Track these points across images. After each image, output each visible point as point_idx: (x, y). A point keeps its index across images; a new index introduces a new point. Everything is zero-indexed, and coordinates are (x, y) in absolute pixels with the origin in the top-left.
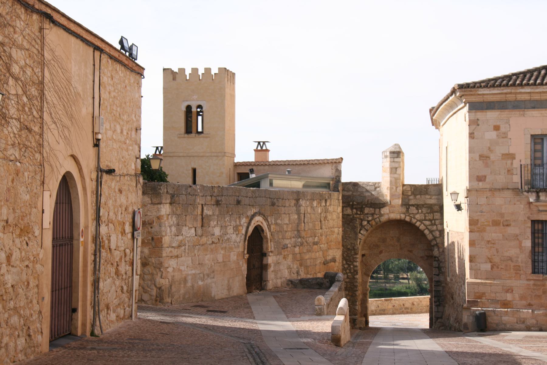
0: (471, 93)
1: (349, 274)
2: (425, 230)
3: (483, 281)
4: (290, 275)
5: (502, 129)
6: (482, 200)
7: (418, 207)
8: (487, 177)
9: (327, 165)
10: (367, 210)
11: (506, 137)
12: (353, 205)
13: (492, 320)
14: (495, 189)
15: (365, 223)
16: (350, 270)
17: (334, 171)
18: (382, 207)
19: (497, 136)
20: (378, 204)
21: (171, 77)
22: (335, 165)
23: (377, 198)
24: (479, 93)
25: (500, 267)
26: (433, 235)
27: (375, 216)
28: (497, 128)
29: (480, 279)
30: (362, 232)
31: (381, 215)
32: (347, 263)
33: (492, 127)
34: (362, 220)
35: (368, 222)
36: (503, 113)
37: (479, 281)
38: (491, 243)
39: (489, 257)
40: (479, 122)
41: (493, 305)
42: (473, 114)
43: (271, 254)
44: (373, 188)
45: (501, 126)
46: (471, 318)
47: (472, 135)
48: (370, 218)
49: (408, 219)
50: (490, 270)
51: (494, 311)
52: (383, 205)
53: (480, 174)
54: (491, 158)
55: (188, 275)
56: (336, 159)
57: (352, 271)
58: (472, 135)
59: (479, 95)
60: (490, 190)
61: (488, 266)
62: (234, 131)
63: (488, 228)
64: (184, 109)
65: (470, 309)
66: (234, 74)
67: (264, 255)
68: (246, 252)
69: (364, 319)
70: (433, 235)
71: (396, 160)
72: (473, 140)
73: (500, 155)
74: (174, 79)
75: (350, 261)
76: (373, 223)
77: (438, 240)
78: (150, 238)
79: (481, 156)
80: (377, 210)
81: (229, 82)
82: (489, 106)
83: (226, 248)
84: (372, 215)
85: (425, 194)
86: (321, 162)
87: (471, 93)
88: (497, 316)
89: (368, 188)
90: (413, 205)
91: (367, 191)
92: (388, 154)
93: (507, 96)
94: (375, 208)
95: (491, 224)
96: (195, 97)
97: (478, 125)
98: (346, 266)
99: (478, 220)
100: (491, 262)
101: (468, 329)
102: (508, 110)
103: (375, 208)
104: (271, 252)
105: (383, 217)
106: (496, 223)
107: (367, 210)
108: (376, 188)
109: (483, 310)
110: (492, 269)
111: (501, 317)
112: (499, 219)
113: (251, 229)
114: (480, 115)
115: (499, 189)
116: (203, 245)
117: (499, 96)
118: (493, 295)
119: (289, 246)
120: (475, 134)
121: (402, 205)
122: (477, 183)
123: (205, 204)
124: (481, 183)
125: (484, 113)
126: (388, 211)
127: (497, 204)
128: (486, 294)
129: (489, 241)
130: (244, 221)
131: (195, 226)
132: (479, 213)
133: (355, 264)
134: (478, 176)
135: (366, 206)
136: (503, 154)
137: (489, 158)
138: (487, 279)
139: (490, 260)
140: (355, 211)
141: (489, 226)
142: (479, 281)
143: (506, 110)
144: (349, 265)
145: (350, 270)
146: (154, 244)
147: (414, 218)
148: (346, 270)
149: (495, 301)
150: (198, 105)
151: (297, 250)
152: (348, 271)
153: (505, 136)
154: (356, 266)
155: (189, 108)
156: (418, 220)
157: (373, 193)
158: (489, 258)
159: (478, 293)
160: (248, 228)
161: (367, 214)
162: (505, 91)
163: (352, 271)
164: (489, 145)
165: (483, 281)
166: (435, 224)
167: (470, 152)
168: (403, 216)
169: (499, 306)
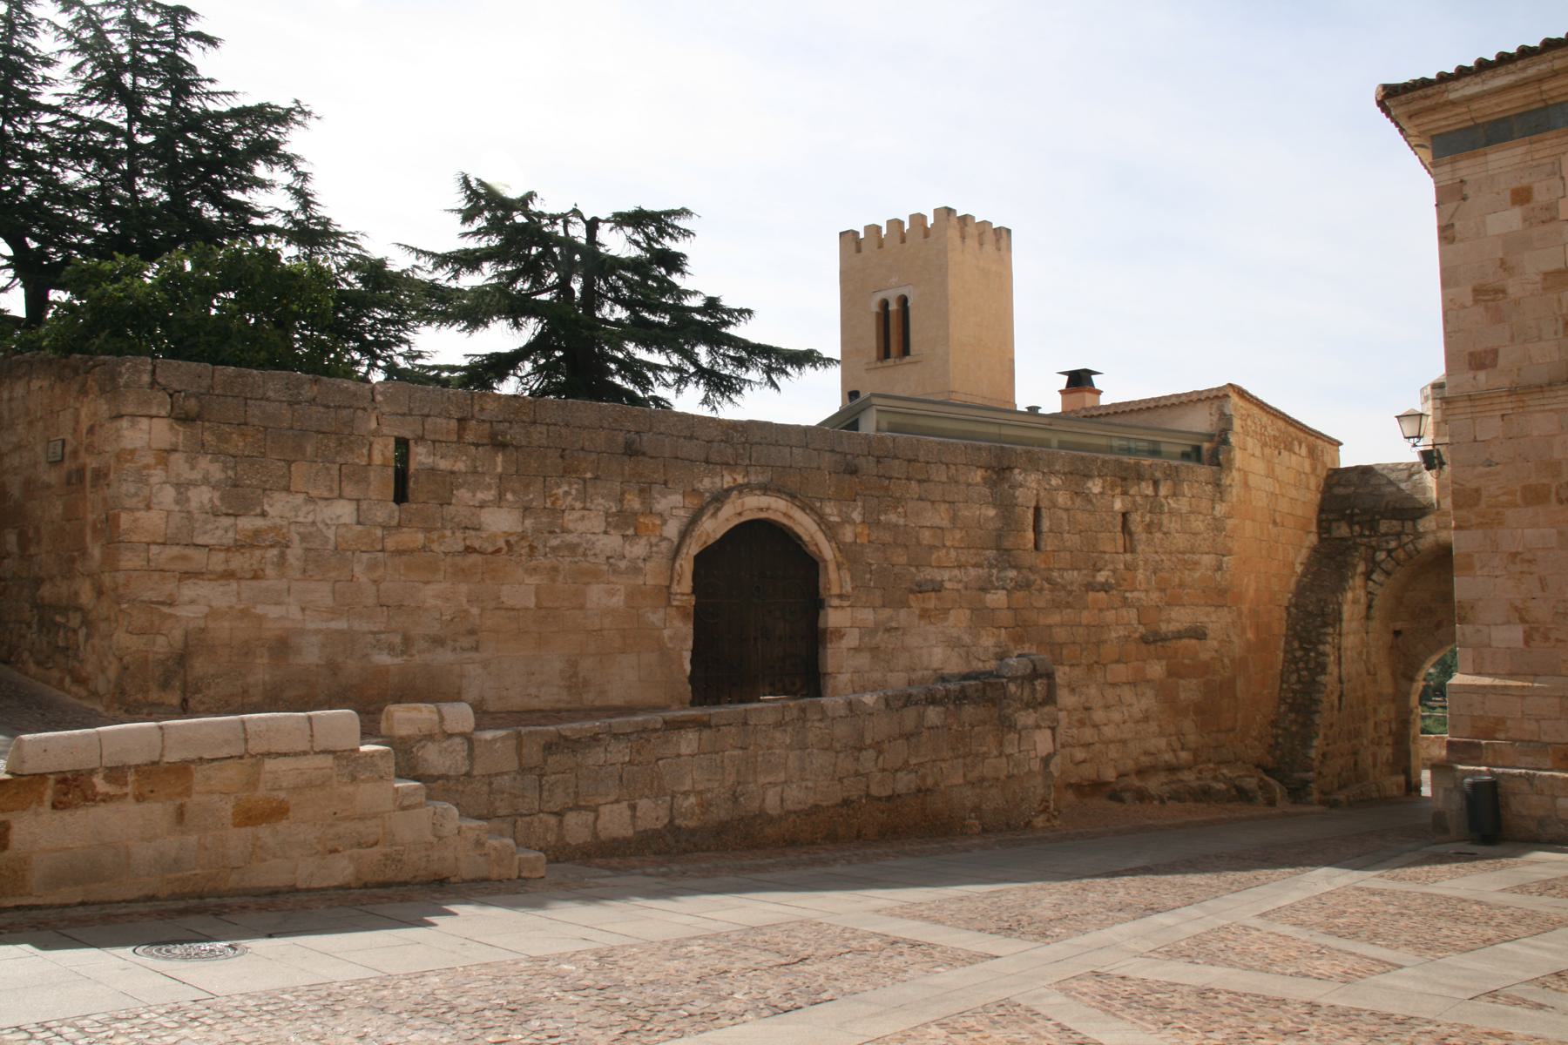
0: (1427, 103)
1: (1304, 673)
3: (1497, 682)
4: (968, 662)
5: (1541, 197)
6: (1490, 427)
8: (1501, 352)
9: (1199, 405)
10: (1384, 526)
11: (1553, 219)
12: (1352, 515)
13: (1525, 806)
14: (1529, 387)
15: (1381, 556)
16: (1306, 663)
17: (1215, 418)
18: (1420, 517)
19: (1525, 220)
20: (1411, 511)
21: (853, 246)
22: (1216, 403)
23: (1410, 498)
24: (1452, 96)
25: (1554, 635)
27: (1405, 539)
28: (1521, 196)
29: (1489, 675)
30: (1374, 577)
31: (1418, 535)
32: (1301, 648)
33: (1508, 193)
34: (1375, 549)
35: (1389, 552)
36: (1538, 146)
37: (1486, 681)
38: (1524, 561)
39: (1518, 603)
40: (1467, 190)
41: (1529, 759)
42: (1447, 168)
43: (835, 602)
44: (1406, 474)
45: (1536, 187)
47: (1448, 233)
48: (1393, 544)
50: (1521, 644)
51: (1529, 779)
52: (1422, 511)
53: (1479, 348)
54: (1510, 290)
56: (1219, 389)
57: (1312, 665)
58: (1447, 233)
59: (1453, 103)
60: (1512, 392)
61: (1516, 634)
62: (1012, 351)
63: (1509, 512)
64: (874, 307)
66: (1009, 231)
67: (815, 604)
69: (1401, 779)
72: (1450, 247)
73: (1538, 278)
74: (859, 250)
75: (1310, 642)
76: (1401, 555)
79: (1478, 292)
80: (1409, 524)
81: (972, 243)
82: (1495, 133)
83: (555, 569)
84: (1398, 535)
86: (1183, 399)
87: (1427, 103)
88: (1541, 793)
89: (1393, 476)
91: (1390, 483)
92: (1429, 391)
93: (1545, 87)
94: (1403, 521)
95: (1519, 501)
96: (894, 280)
97: (1464, 199)
98: (1299, 654)
99: (1477, 490)
100: (1523, 620)
102: (1555, 132)
103: (1403, 521)
104: (840, 596)
105: (1422, 541)
106: (1535, 496)
107: (1384, 526)
108: (1411, 475)
109: (1492, 773)
110: (1526, 642)
111: (1554, 797)
112: (1544, 481)
113: (714, 527)
114: (1467, 168)
115: (1540, 388)
117: (1517, 94)
118: (1533, 726)
119: (948, 585)
120: (1457, 226)
122: (1471, 374)
123: (421, 439)
124: (1482, 375)
125: (1481, 160)
126: (1433, 525)
127: (1535, 433)
128: (1509, 723)
129: (1514, 555)
130: (672, 503)
132: (1481, 469)
133: (1321, 647)
134: (1471, 354)
135: (1383, 517)
136: (1546, 275)
137: (1503, 291)
138: (1512, 675)
139: (1520, 614)
140: (1357, 528)
141: (1514, 505)
142: (1486, 681)
143: (1549, 135)
144: (1307, 651)
145: (1306, 663)
148: (1296, 664)
149: (1535, 747)
152: (1301, 665)
153: (1550, 215)
154: (1324, 654)
157: (1403, 486)
158: (1516, 609)
159: (1481, 718)
160: (694, 521)
161: (1386, 534)
162: (1531, 72)
163: (1312, 665)
164: (1500, 255)
165: (1497, 682)
167: (1445, 284)
169: (1549, 764)
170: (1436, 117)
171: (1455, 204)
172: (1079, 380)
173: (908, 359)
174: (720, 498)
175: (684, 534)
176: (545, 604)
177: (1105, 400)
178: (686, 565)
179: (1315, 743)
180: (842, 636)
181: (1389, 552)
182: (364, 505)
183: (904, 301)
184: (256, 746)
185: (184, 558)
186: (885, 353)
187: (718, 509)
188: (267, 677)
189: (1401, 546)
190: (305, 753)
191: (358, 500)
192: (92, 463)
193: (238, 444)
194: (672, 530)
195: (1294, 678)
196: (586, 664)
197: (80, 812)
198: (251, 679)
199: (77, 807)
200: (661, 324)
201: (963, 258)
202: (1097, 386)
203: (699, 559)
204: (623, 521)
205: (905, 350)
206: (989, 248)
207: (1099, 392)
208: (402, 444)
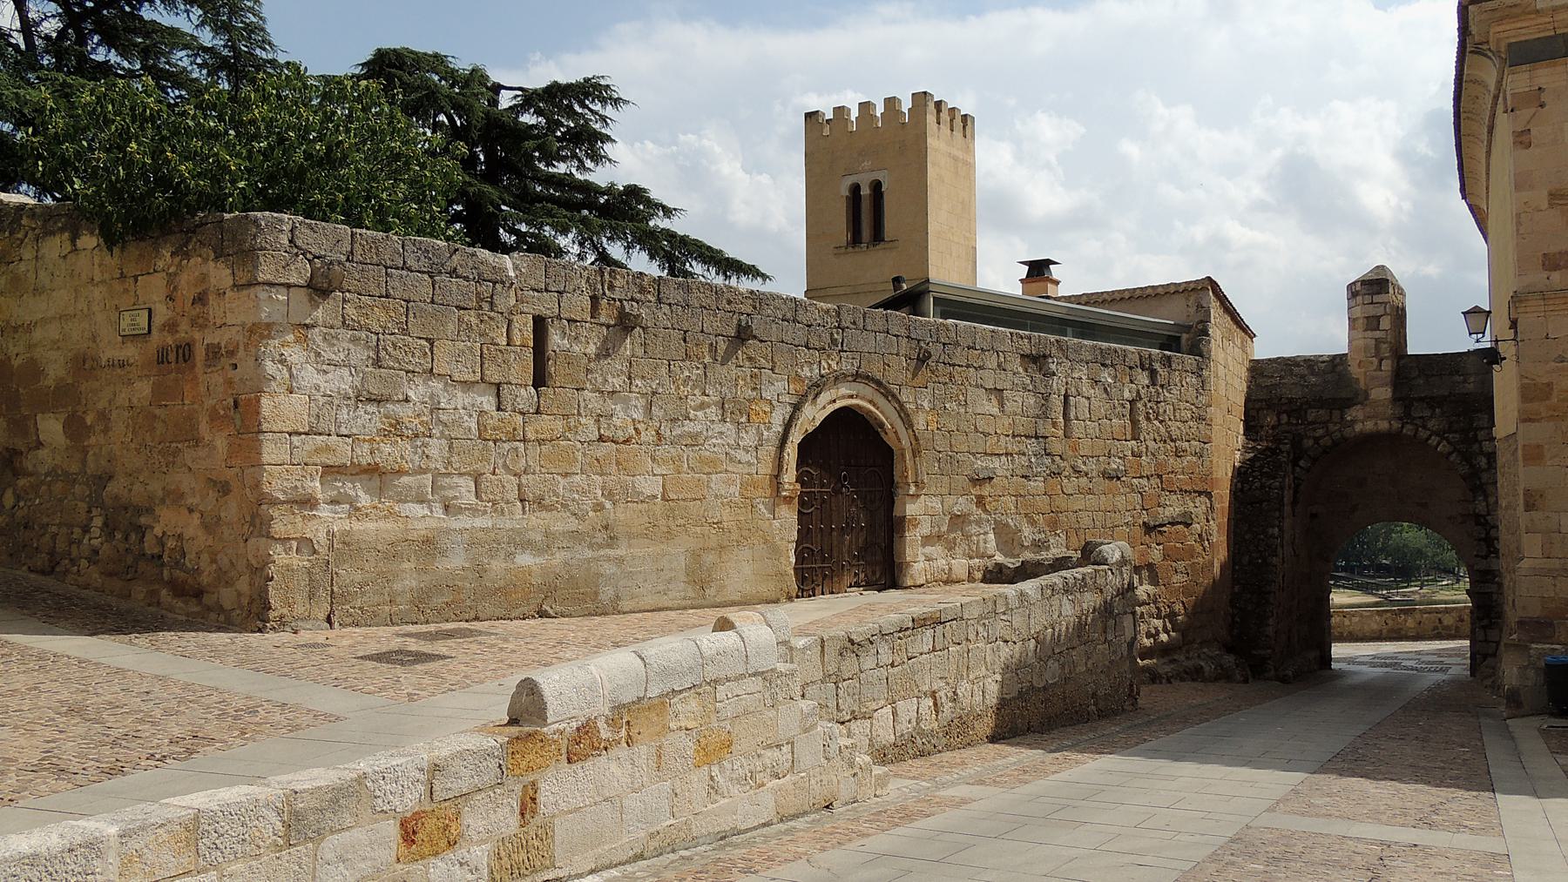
2: (1450, 454)
7: (1432, 402)
10: (1312, 415)
17: (1192, 310)
26: (1472, 466)
40: (1544, 97)
46: (1531, 673)
48: (1320, 432)
49: (1408, 430)
53: (1553, 249)
55: (448, 531)
65: (1527, 648)
68: (790, 476)
70: (1472, 466)
71: (1377, 298)
77: (1485, 477)
78: (231, 401)
79: (1553, 196)
81: (945, 128)
85: (1451, 374)
86: (1160, 290)
90: (1421, 399)
99: (1549, 385)
101: (1519, 705)
107: (1312, 415)
113: (814, 415)
116: (540, 442)
121: (1395, 399)
130: (778, 388)
131: (494, 375)
146: (238, 423)
147: (1424, 427)
150: (871, 180)
151: (1037, 485)
155: (856, 189)
156: (1433, 433)
160: (797, 408)
161: (1313, 423)
166: (1475, 440)
168: (1396, 425)
170: (1519, 25)
171: (1533, 110)
172: (1038, 270)
173: (882, 245)
174: (817, 387)
175: (788, 426)
176: (673, 496)
177: (1062, 291)
178: (791, 453)
179: (1271, 621)
180: (915, 526)
181: (1316, 440)
182: (505, 390)
183: (877, 187)
184: (711, 672)
185: (328, 449)
186: (856, 240)
187: (817, 396)
188: (414, 583)
189: (1328, 434)
190: (742, 676)
191: (498, 385)
192: (204, 339)
193: (378, 318)
194: (778, 418)
195: (1246, 559)
196: (710, 558)
197: (588, 764)
198: (397, 586)
199: (587, 756)
200: (21, 207)
201: (938, 142)
202: (1055, 276)
203: (802, 446)
204: (735, 411)
205: (878, 236)
206: (958, 134)
207: (1057, 283)
208: (540, 324)
